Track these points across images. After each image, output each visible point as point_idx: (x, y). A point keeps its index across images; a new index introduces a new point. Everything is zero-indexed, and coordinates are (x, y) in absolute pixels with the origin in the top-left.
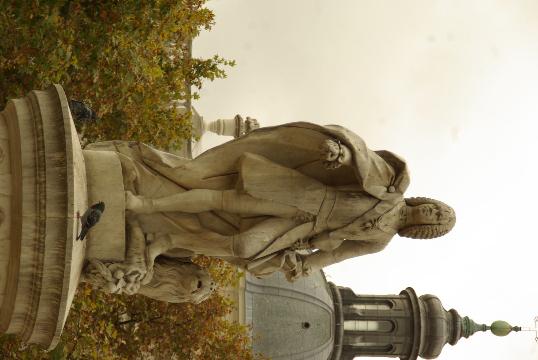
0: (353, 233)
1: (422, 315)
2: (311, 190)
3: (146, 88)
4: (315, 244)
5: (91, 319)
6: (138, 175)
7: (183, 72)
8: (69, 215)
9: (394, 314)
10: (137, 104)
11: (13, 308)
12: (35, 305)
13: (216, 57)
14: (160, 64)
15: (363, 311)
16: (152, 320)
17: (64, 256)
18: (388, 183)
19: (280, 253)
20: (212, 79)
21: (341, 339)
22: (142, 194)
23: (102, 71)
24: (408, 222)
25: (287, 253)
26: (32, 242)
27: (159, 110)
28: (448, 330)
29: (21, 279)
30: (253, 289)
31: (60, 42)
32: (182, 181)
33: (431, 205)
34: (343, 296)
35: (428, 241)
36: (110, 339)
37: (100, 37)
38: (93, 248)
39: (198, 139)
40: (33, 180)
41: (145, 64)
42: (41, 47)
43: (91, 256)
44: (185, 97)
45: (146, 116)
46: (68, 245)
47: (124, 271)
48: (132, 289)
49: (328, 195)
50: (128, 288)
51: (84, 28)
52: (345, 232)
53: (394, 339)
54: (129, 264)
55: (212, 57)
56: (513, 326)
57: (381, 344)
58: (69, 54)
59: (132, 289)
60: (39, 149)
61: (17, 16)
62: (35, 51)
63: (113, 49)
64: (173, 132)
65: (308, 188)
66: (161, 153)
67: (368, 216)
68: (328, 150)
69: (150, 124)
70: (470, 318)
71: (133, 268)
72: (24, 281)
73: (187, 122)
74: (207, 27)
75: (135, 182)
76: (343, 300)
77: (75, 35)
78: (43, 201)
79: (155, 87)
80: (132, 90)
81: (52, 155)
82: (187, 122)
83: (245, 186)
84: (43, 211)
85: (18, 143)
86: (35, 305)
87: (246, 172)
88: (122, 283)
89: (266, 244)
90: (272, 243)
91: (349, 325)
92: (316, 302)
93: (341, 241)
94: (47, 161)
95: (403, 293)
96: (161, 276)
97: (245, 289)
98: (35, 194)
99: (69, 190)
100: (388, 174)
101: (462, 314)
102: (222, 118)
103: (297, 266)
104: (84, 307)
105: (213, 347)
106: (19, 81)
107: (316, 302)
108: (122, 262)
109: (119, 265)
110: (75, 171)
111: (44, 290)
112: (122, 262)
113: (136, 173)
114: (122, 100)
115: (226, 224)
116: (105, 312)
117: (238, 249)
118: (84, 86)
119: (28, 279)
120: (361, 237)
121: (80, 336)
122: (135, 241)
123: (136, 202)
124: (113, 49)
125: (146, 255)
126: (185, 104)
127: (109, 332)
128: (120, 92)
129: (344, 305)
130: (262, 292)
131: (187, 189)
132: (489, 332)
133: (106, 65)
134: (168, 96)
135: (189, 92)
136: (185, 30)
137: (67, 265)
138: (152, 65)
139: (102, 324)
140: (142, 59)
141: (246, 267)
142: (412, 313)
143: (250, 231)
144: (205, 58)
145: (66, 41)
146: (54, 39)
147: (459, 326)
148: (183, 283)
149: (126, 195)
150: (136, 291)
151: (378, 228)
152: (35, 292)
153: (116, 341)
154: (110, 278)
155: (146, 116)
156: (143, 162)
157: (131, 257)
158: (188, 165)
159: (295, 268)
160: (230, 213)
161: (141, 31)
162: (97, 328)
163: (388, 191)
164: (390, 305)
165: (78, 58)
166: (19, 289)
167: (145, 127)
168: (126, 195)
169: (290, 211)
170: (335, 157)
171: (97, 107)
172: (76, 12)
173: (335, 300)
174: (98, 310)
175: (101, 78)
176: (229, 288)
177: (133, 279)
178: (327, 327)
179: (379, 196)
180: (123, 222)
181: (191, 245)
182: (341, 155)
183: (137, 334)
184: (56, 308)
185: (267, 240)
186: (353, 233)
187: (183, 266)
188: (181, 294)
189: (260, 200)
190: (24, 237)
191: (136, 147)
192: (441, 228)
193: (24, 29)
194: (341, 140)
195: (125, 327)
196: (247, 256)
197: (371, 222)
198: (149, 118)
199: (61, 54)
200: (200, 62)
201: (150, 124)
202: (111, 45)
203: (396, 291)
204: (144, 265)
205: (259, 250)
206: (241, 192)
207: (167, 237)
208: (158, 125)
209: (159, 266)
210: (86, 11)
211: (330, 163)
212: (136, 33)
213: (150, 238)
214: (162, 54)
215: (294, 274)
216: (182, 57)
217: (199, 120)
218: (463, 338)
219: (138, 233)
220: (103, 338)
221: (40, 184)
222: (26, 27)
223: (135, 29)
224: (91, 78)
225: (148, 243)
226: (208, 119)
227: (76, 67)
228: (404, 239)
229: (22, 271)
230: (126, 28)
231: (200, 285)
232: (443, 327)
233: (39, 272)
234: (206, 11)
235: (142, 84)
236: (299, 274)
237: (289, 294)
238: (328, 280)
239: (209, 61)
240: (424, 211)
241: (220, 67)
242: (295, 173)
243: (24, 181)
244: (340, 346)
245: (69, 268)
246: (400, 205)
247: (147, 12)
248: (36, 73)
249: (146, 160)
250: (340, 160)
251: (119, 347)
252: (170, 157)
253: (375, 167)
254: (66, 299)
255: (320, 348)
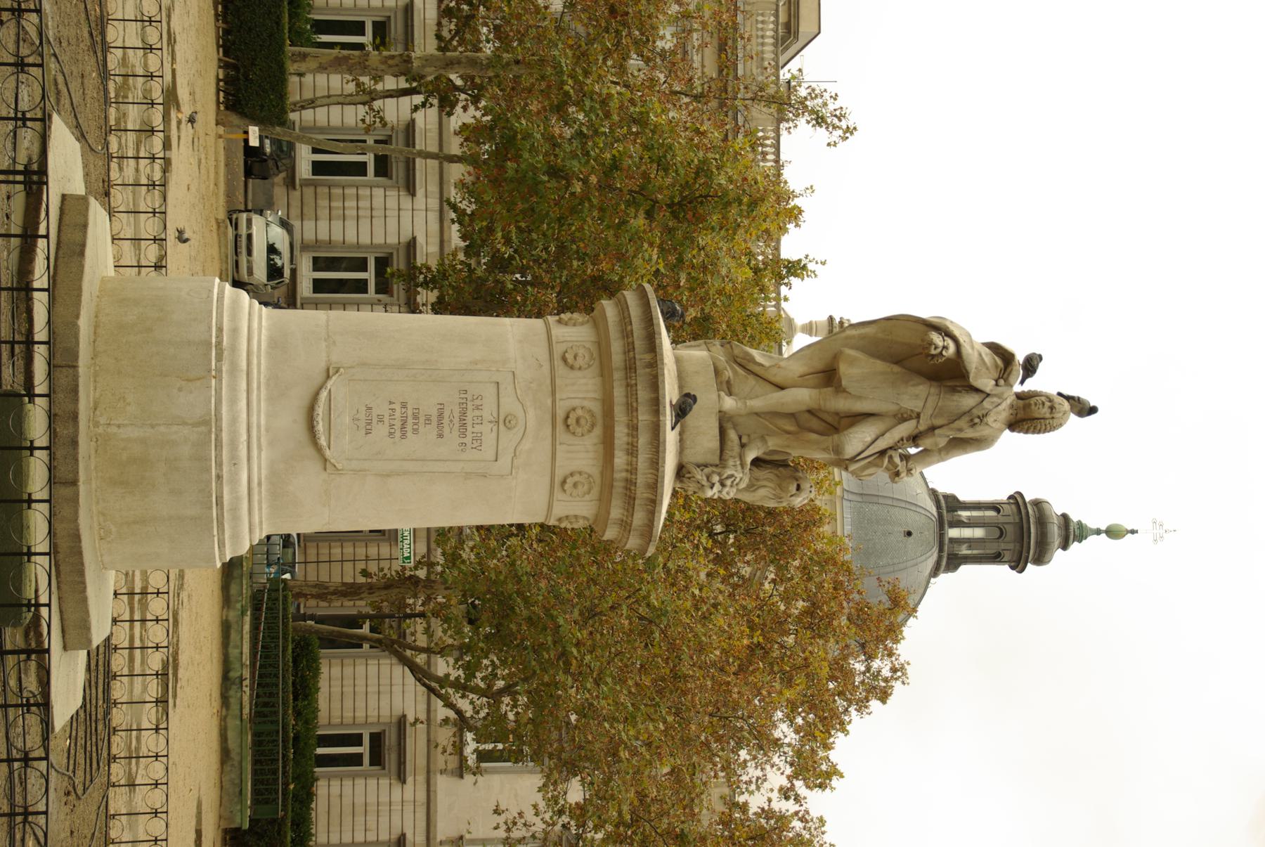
0: (960, 430)
1: (1032, 520)
2: (913, 385)
3: (735, 289)
4: (920, 442)
5: (685, 529)
6: (731, 375)
7: (773, 273)
8: (661, 418)
9: (1001, 519)
10: (725, 307)
11: (609, 513)
12: (631, 510)
13: (807, 257)
14: (748, 264)
15: (969, 518)
16: (747, 531)
17: (658, 459)
18: (996, 376)
19: (882, 453)
20: (803, 279)
21: (946, 548)
22: (736, 395)
23: (689, 274)
24: (1019, 416)
25: (890, 452)
26: (626, 447)
27: (748, 313)
28: (1060, 535)
29: (615, 484)
30: (851, 497)
31: (646, 245)
32: (777, 380)
33: (1043, 399)
34: (946, 502)
35: (1041, 436)
36: (705, 549)
37: (686, 238)
38: (687, 452)
39: (788, 343)
40: (624, 383)
41: (733, 264)
42: (627, 251)
43: (685, 460)
44: (774, 299)
45: (736, 319)
46: (661, 449)
47: (720, 474)
48: (728, 493)
49: (933, 390)
50: (724, 492)
51: (670, 231)
52: (952, 429)
53: (1003, 546)
54: (724, 467)
55: (802, 257)
56: (1129, 529)
57: (988, 552)
58: (655, 257)
59: (728, 493)
60: (629, 351)
61: (603, 221)
62: (621, 257)
63: (700, 250)
64: (763, 335)
65: (912, 383)
66: (756, 354)
67: (975, 412)
68: (931, 343)
69: (739, 328)
70: (1083, 522)
71: (729, 472)
72: (619, 487)
73: (777, 325)
74: (797, 225)
75: (728, 382)
76: (947, 507)
77: (660, 238)
78: (635, 404)
79: (745, 289)
80: (720, 292)
81: (642, 356)
82: (777, 325)
83: (844, 383)
84: (635, 414)
85: (609, 345)
86: (631, 510)
87: (844, 369)
88: (717, 487)
89: (867, 444)
90: (873, 442)
91: (953, 533)
92: (918, 510)
93: (947, 439)
94: (638, 363)
95: (1010, 497)
96: (757, 480)
97: (843, 498)
98: (627, 397)
99: (661, 392)
100: (997, 366)
101: (1074, 517)
102: (814, 320)
103: (901, 466)
104: (677, 516)
105: (811, 559)
106: (605, 289)
107: (918, 510)
108: (717, 466)
109: (714, 469)
110: (666, 372)
111: (639, 494)
112: (717, 466)
113: (728, 373)
114: (709, 303)
115: (823, 424)
116: (699, 522)
117: (838, 450)
118: (670, 290)
119: (622, 484)
120: (969, 433)
121: (675, 547)
122: (729, 443)
123: (729, 403)
124: (700, 250)
125: (741, 457)
126: (774, 306)
127: (704, 541)
128: (708, 294)
129: (948, 511)
130: (860, 499)
131: (782, 388)
132: (1104, 535)
133: (693, 267)
134: (757, 299)
135: (779, 294)
136: (773, 228)
137: (661, 469)
138: (741, 265)
139: (697, 534)
140: (730, 259)
141: (846, 469)
142: (1021, 518)
143: (851, 430)
144: (794, 258)
145: (651, 245)
146: (639, 242)
147: (1072, 531)
148: (780, 486)
149: (719, 396)
150: (732, 495)
151: (987, 424)
152: (630, 497)
153: (711, 552)
154: (704, 482)
155: (736, 319)
156: (736, 362)
157: (726, 461)
158: (783, 364)
159: (899, 468)
160: (828, 413)
161: (727, 230)
162: (692, 538)
163: (997, 385)
164: (998, 511)
165: (664, 261)
166: (614, 495)
167: (734, 331)
168: (719, 396)
169: (892, 408)
170: (939, 350)
171: (685, 309)
172: (662, 214)
173: (939, 507)
174: (693, 520)
175: (687, 280)
176: (827, 496)
177: (728, 482)
178: (930, 534)
179: (988, 390)
180: (717, 425)
181: (788, 446)
182: (945, 348)
183: (732, 545)
184: (654, 503)
185: (869, 439)
186: (960, 430)
187: (781, 469)
188: (779, 498)
189: (860, 398)
190: (617, 442)
191: (728, 346)
192: (1055, 422)
193: (610, 234)
194: (947, 333)
195: (720, 538)
196: (847, 457)
197: (979, 417)
198: (738, 322)
199: (647, 258)
200: (789, 262)
201: (739, 328)
202: (698, 246)
203: (1001, 495)
204: (739, 468)
205: (860, 449)
206: (839, 389)
207: (763, 439)
208: (748, 328)
209: (755, 469)
210: (671, 213)
211: (933, 356)
212: (723, 232)
213: (744, 440)
214: (750, 254)
215: (897, 474)
216: (771, 257)
217: (790, 321)
218: (1076, 543)
219: (732, 435)
220: (698, 549)
221: (632, 386)
222: (612, 232)
223: (721, 229)
224: (678, 281)
225: (743, 446)
226: (800, 320)
227: (662, 270)
228: (1015, 434)
229: (617, 476)
230: (713, 229)
231: (798, 488)
232: (1055, 532)
233: (634, 477)
234: (796, 207)
235: (731, 285)
236: (903, 475)
237: (890, 502)
238: (931, 486)
239: (800, 261)
240: (1036, 404)
241: (811, 266)
242: (896, 368)
243: (615, 384)
244: (945, 555)
245: (664, 472)
246: (1010, 399)
247: (734, 211)
248: (622, 278)
249: (739, 360)
250: (944, 353)
251: (714, 559)
252: (764, 355)
253: (982, 360)
254: (661, 503)
255: (924, 557)
